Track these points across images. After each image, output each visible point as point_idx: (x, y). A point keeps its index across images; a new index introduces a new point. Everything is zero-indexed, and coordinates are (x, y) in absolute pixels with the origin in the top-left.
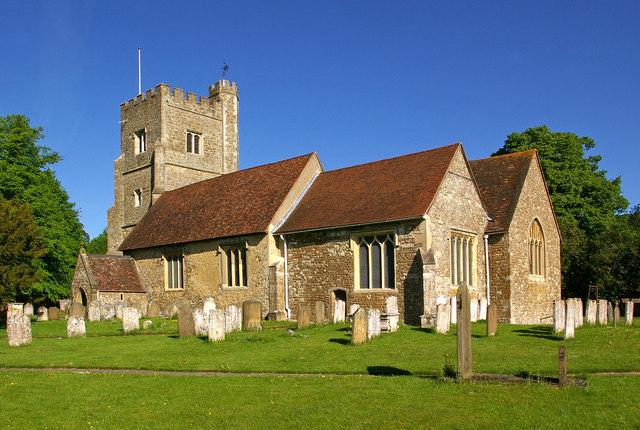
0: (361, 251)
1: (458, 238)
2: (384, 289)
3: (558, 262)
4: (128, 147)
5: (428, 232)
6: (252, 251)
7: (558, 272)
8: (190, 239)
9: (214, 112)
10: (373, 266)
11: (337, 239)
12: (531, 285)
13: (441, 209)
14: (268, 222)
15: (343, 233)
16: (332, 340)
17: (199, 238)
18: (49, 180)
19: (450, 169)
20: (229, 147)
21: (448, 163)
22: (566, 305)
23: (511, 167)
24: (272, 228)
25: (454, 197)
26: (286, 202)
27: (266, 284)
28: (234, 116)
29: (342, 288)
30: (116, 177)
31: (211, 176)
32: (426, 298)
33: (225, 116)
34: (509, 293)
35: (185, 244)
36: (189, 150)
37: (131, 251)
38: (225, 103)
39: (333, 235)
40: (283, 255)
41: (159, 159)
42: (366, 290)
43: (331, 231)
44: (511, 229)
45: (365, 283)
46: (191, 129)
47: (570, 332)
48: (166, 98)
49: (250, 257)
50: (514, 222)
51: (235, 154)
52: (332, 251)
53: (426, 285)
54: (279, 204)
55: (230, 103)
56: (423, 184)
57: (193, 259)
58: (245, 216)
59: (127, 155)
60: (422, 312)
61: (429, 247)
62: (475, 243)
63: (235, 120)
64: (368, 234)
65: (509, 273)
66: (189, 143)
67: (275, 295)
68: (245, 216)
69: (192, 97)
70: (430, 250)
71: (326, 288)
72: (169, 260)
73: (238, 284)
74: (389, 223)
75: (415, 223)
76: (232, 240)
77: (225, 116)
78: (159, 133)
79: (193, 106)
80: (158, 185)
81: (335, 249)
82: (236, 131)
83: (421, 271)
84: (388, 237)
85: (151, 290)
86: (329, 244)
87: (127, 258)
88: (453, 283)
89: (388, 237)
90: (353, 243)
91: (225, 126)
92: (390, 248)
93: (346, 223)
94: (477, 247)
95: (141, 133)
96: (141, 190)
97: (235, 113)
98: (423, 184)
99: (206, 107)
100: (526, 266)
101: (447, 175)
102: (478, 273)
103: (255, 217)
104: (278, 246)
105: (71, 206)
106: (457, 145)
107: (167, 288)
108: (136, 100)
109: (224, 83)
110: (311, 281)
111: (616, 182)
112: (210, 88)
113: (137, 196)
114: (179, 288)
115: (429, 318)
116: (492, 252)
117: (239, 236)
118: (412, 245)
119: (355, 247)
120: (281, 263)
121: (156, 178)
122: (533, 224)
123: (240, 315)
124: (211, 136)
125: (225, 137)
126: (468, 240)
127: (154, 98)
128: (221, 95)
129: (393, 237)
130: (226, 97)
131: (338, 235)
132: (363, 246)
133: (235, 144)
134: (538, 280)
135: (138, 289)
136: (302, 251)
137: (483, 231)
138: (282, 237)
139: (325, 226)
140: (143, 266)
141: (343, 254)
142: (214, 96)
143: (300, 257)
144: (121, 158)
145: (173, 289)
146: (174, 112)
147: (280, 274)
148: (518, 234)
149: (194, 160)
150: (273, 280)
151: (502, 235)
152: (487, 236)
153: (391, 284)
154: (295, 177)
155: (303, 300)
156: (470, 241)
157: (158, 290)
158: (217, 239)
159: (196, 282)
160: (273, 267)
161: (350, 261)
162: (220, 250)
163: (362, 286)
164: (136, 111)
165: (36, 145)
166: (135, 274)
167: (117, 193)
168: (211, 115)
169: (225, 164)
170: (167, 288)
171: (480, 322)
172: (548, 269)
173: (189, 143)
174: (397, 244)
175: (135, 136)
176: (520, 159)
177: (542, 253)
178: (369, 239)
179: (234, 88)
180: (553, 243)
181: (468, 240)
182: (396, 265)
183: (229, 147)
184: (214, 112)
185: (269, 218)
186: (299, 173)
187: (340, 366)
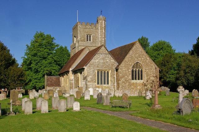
12: (133, 84)
24: (71, 69)
26: (79, 62)
28: (103, 27)
31: (97, 47)
77: (99, 28)
95: (75, 37)
115: (83, 94)
124: (95, 35)
125: (100, 35)
130: (100, 22)
146: (82, 30)
149: (88, 43)
168: (95, 28)
184: (95, 27)
185: (70, 67)
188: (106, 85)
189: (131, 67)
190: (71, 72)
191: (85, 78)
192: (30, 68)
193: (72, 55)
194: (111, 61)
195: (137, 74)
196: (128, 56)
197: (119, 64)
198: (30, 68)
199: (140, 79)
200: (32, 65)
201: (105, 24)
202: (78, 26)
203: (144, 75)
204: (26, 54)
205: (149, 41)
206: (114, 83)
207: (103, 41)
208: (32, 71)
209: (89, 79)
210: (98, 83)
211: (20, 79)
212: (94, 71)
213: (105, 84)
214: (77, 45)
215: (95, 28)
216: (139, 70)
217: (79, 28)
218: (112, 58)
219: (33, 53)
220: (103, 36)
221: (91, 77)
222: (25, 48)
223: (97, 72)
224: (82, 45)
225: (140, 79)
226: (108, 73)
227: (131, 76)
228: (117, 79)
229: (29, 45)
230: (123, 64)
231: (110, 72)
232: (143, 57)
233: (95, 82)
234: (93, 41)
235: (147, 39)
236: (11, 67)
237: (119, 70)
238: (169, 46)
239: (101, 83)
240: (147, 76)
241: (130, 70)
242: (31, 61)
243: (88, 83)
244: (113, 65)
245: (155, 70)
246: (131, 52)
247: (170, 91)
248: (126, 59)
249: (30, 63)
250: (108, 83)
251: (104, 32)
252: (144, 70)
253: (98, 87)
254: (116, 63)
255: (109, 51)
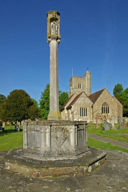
24: (65, 107)
77: (86, 79)
146: (75, 81)
188: (85, 117)
189: (101, 105)
190: (65, 109)
191: (72, 113)
192: (44, 107)
193: (69, 97)
194: (89, 101)
195: (105, 110)
196: (99, 98)
197: (94, 103)
198: (44, 107)
200: (45, 105)
201: (90, 77)
202: (73, 79)
203: (110, 110)
204: (42, 98)
205: (122, 86)
206: (91, 116)
207: (89, 88)
208: (45, 108)
209: (75, 113)
210: (80, 116)
211: (36, 113)
212: (77, 108)
213: (85, 116)
214: (72, 91)
216: (106, 107)
217: (73, 80)
218: (89, 100)
219: (45, 97)
220: (89, 85)
221: (76, 112)
222: (41, 94)
223: (79, 109)
226: (87, 109)
227: (101, 111)
228: (92, 113)
229: (43, 92)
230: (96, 103)
231: (88, 109)
232: (109, 99)
233: (78, 115)
235: (121, 85)
236: (31, 106)
237: (94, 107)
238: (27, 95)
239: (83, 116)
240: (112, 111)
241: (101, 107)
242: (44, 102)
243: (74, 116)
244: (89, 104)
245: (117, 107)
246: (101, 96)
248: (98, 100)
249: (44, 104)
250: (87, 116)
251: (89, 82)
252: (110, 107)
253: (81, 118)
254: (92, 103)
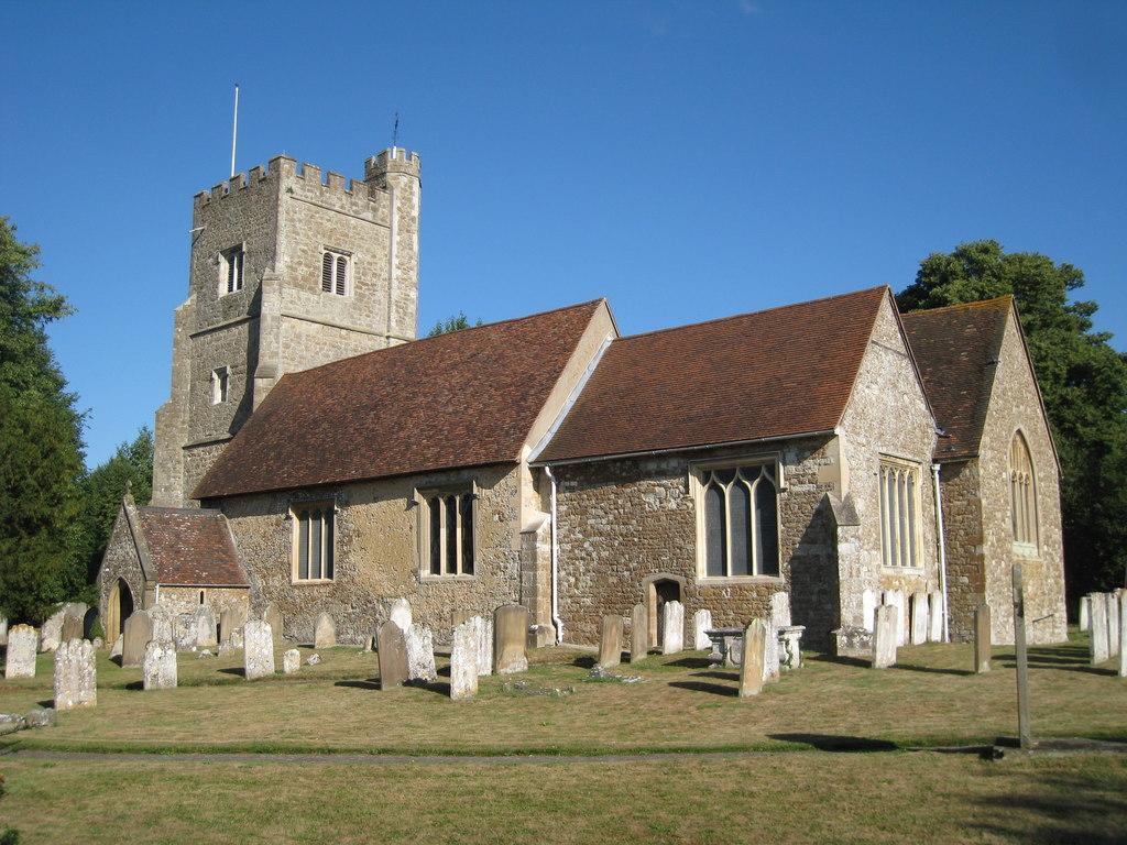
0: (707, 498)
1: (891, 471)
2: (757, 576)
3: (1057, 515)
4: (203, 282)
5: (843, 460)
6: (486, 498)
7: (1057, 535)
8: (353, 474)
9: (375, 210)
10: (734, 531)
11: (661, 474)
13: (861, 415)
14: (520, 441)
15: (674, 463)
16: (671, 684)
17: (373, 472)
18: (37, 356)
19: (873, 337)
20: (402, 280)
21: (867, 325)
22: (1107, 603)
23: (970, 330)
24: (528, 453)
25: (882, 390)
27: (513, 568)
28: (413, 219)
29: (670, 576)
30: (176, 343)
32: (844, 595)
33: (396, 218)
34: (983, 579)
35: (342, 484)
36: (327, 287)
37: (218, 497)
38: (397, 192)
39: (652, 466)
40: (546, 507)
41: (271, 306)
42: (719, 580)
43: (649, 458)
44: (981, 452)
45: (718, 566)
46: (332, 244)
47: (885, 656)
48: (288, 181)
49: (480, 513)
50: (985, 439)
51: (413, 294)
52: (650, 499)
53: (843, 566)
54: (541, 404)
55: (406, 190)
56: (826, 365)
57: (359, 516)
58: (470, 429)
59: (201, 298)
60: (837, 623)
61: (845, 491)
62: (919, 481)
63: (415, 227)
64: (724, 464)
65: (981, 540)
66: (327, 273)
67: (534, 592)
68: (470, 429)
69: (336, 181)
70: (848, 497)
71: (638, 575)
72: (303, 517)
73: (452, 568)
74: (766, 443)
75: (817, 442)
76: (442, 478)
77: (396, 218)
78: (271, 254)
79: (337, 199)
80: (265, 359)
81: (656, 495)
82: (416, 247)
83: (832, 540)
84: (764, 471)
85: (260, 583)
86: (644, 484)
87: (210, 513)
88: (885, 562)
89: (764, 471)
90: (694, 482)
91: (396, 238)
92: (768, 494)
93: (681, 443)
94: (923, 485)
95: (234, 253)
96: (229, 371)
97: (415, 213)
98: (826, 365)
99: (361, 199)
100: (1008, 525)
101: (869, 347)
102: (926, 543)
103: (492, 430)
104: (537, 487)
105: (72, 399)
106: (881, 290)
107: (295, 579)
108: (226, 185)
109: (395, 154)
110: (610, 562)
111: (56, 307)
112: (368, 162)
113: (217, 382)
114: (324, 579)
115: (850, 636)
116: (947, 500)
117: (458, 469)
118: (811, 487)
119: (698, 490)
120: (545, 525)
121: (263, 344)
122: (1014, 441)
123: (490, 635)
124: (368, 258)
125: (395, 261)
126: (907, 474)
127: (260, 189)
128: (390, 177)
129: (773, 471)
131: (664, 466)
132: (715, 492)
133: (414, 276)
134: (1027, 552)
135: (233, 580)
136: (588, 497)
137: (929, 456)
138: (547, 469)
139: (637, 448)
140: (244, 532)
141: (673, 505)
142: (375, 178)
143: (584, 512)
144: (188, 303)
145: (310, 580)
146: (302, 211)
147: (543, 548)
148: (994, 462)
149: (333, 307)
150: (529, 560)
151: (964, 464)
152: (937, 467)
153: (770, 566)
154: (568, 349)
155: (588, 601)
156: (911, 477)
157: (276, 582)
158: (411, 475)
159: (361, 563)
160: (531, 534)
161: (687, 520)
162: (417, 497)
163: (711, 572)
164: (226, 207)
165: (23, 279)
166: (227, 550)
167: (176, 373)
169: (394, 316)
170: (295, 579)
171: (928, 642)
172: (1042, 529)
173: (327, 273)
174: (782, 486)
175: (222, 259)
176: (984, 314)
177: (1031, 498)
178: (726, 476)
179: (415, 164)
180: (1047, 478)
181: (907, 474)
182: (780, 527)
183: (402, 280)
184: (375, 210)
186: (576, 341)
187: (109, 734)
199: (184, 663)
202: (284, 185)
215: (369, 216)
224: (298, 314)
225: (184, 663)
234: (360, 297)
247: (898, 649)
255: (622, 335)
